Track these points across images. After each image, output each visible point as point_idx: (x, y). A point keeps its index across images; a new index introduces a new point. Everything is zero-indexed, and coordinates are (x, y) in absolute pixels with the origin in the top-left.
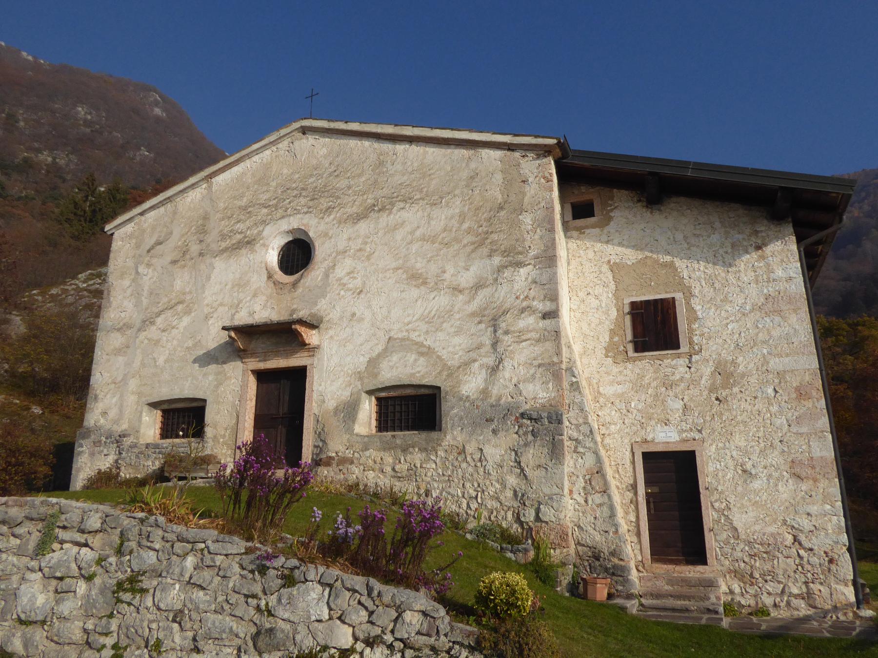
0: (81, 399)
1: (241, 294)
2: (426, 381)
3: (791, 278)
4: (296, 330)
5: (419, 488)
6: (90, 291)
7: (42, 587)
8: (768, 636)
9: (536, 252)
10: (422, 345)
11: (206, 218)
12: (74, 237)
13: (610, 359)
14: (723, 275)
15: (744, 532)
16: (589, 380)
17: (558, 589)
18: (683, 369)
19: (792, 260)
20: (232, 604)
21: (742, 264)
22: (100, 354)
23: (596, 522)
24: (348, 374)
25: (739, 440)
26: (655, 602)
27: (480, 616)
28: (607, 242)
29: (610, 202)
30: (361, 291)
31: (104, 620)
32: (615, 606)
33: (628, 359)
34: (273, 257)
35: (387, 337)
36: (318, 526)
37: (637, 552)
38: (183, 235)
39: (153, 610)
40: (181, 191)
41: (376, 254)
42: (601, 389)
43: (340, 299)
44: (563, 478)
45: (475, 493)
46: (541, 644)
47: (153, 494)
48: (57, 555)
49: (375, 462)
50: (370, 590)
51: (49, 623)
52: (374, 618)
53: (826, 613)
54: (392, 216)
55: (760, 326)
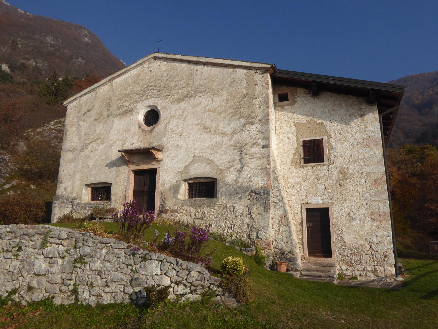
0: (54, 182)
1: (127, 135)
3: (375, 131)
4: (152, 152)
5: (206, 223)
6: (56, 130)
7: (43, 261)
8: (353, 287)
10: (208, 159)
11: (110, 99)
12: (47, 103)
13: (293, 166)
14: (345, 128)
15: (348, 244)
16: (283, 176)
17: (265, 267)
18: (325, 171)
19: (376, 122)
20: (121, 268)
21: (354, 123)
22: (63, 162)
23: (283, 239)
24: (175, 172)
25: (348, 203)
26: (307, 273)
27: (223, 274)
28: (294, 113)
29: (296, 94)
30: (181, 134)
31: (70, 274)
32: (288, 274)
33: (301, 166)
34: (141, 118)
35: (193, 156)
36: (157, 238)
37: (302, 252)
39: (89, 270)
40: (98, 86)
42: (289, 180)
44: (269, 219)
45: (231, 226)
46: (246, 285)
47: (89, 224)
48: (49, 249)
50: (177, 263)
51: (47, 275)
52: (179, 274)
53: (382, 278)
54: (195, 100)
55: (360, 152)
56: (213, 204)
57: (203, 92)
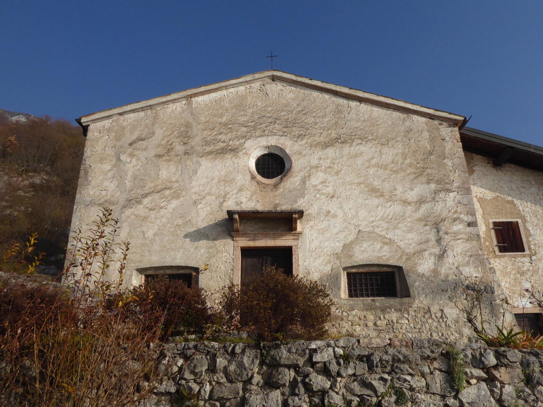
2: (392, 262)
9: (457, 184)
24: (327, 255)
29: (472, 161)
33: (496, 256)
38: (166, 137)
40: (163, 103)
41: (343, 172)
43: (316, 200)
49: (360, 319)
56: (407, 307)
57: (364, 139)
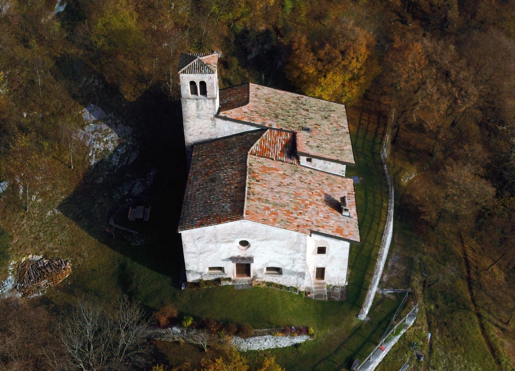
57: (274, 239)
